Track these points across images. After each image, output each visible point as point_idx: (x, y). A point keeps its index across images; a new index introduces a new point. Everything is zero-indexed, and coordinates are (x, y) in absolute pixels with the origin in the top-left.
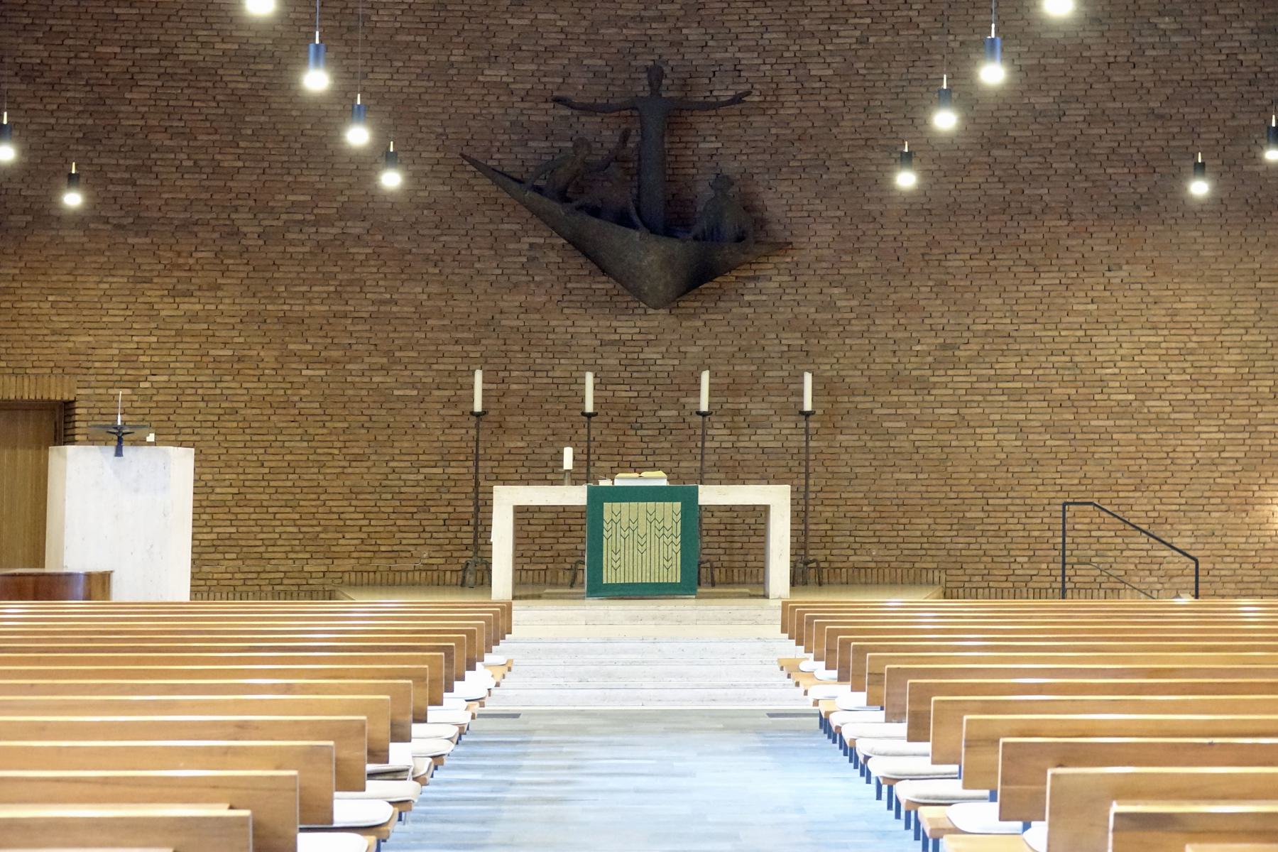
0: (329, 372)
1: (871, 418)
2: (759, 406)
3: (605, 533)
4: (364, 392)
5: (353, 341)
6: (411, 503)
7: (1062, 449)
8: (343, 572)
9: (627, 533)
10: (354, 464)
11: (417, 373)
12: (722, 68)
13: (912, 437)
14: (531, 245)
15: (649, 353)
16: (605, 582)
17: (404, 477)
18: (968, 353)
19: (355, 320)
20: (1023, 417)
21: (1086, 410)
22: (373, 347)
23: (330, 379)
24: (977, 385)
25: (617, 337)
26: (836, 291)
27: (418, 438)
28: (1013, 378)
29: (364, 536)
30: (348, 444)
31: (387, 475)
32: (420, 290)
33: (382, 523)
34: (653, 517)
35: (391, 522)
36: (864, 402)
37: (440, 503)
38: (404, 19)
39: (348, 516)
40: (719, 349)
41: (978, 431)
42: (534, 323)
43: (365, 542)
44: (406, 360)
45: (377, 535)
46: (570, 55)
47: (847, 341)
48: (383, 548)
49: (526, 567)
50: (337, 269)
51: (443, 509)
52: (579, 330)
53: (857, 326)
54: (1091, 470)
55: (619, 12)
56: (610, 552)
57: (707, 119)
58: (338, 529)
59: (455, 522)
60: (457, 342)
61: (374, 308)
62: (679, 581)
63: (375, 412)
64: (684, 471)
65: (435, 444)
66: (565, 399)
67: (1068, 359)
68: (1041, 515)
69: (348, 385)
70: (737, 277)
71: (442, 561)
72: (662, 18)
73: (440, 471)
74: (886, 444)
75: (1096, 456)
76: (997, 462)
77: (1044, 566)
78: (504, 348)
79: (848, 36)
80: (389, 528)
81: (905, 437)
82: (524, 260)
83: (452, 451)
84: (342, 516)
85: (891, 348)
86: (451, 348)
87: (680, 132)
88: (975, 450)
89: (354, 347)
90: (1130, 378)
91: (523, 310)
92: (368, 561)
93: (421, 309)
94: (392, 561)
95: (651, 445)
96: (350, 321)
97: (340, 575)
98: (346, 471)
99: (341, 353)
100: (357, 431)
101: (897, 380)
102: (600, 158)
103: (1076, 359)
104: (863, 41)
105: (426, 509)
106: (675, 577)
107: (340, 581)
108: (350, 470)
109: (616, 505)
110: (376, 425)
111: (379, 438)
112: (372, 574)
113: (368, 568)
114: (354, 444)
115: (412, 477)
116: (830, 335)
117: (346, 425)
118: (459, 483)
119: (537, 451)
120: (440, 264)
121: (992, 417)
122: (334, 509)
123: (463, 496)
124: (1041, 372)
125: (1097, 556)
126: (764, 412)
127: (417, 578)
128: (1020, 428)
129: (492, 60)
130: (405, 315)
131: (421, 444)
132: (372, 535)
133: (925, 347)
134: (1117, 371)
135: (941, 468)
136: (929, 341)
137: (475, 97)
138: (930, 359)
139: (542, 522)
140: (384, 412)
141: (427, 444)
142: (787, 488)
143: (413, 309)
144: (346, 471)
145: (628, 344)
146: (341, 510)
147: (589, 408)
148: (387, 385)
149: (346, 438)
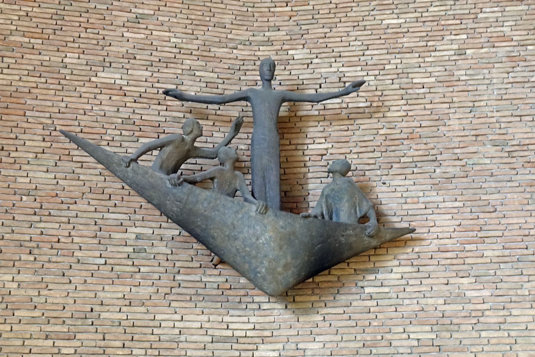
12: (327, 80)
14: (138, 237)
25: (229, 333)
26: (465, 281)
32: (10, 278)
38: (20, 23)
40: (342, 345)
42: (139, 316)
46: (184, 67)
47: (484, 334)
52: (187, 324)
53: (492, 318)
57: (316, 124)
70: (355, 270)
72: (270, 42)
78: (102, 343)
82: (131, 249)
86: (40, 342)
87: (289, 136)
91: (127, 302)
102: (211, 146)
104: (461, 53)
116: (463, 327)
120: (36, 251)
129: (106, 65)
137: (87, 95)
145: (241, 340)
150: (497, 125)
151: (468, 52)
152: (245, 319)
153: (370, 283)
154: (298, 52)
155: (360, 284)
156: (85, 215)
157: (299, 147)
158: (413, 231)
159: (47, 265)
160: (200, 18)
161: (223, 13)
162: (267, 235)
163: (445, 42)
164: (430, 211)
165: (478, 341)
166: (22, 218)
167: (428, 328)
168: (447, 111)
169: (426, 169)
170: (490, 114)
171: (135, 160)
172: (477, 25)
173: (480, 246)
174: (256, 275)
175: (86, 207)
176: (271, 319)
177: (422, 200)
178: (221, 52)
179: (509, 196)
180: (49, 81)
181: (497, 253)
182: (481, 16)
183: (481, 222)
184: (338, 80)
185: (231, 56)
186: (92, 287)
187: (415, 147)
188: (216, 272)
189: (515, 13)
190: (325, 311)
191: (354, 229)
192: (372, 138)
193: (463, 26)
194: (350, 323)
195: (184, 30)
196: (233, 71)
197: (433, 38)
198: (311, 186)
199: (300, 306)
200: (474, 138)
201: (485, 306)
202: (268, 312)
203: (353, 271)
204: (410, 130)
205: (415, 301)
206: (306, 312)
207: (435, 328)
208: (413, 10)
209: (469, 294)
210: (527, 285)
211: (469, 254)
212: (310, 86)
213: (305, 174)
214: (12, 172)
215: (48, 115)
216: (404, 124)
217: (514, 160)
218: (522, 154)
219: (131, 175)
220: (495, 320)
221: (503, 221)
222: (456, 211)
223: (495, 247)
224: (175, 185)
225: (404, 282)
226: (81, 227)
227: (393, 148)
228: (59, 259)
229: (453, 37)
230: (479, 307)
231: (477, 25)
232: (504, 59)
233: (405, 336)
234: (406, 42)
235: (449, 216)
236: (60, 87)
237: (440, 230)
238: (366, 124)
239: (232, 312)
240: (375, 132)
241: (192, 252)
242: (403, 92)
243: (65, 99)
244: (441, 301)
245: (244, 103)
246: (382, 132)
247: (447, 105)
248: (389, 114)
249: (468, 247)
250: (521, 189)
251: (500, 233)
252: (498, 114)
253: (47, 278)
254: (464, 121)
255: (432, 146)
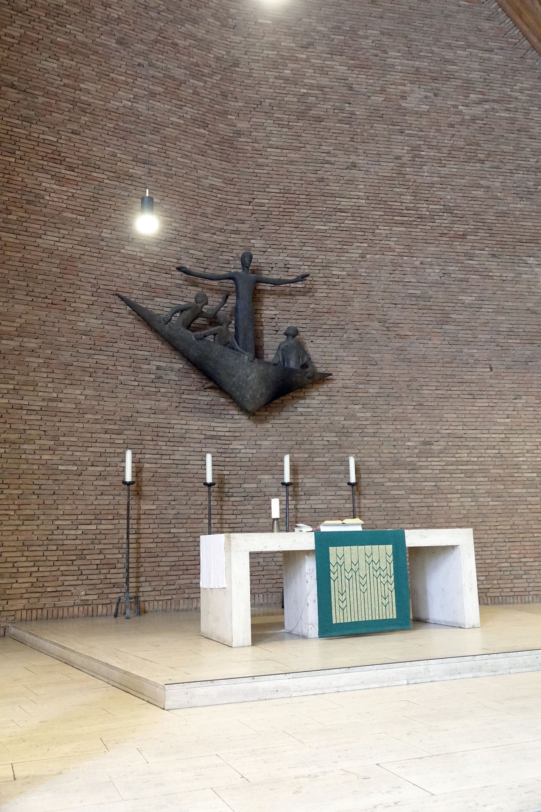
0: (7, 450)
1: (383, 488)
2: (311, 480)
3: (332, 575)
4: (35, 467)
5: (27, 428)
6: (72, 553)
7: (499, 507)
8: (16, 610)
9: (350, 574)
10: (26, 523)
11: (76, 453)
13: (409, 500)
14: (158, 368)
15: (236, 445)
16: (334, 622)
17: (66, 532)
18: (439, 447)
19: (29, 412)
20: (474, 487)
21: (510, 483)
22: (42, 433)
23: (8, 456)
24: (446, 467)
26: (356, 407)
27: (77, 502)
28: (467, 463)
29: (35, 580)
30: (22, 507)
31: (52, 531)
33: (49, 569)
34: (370, 559)
35: (55, 568)
36: (378, 478)
37: (93, 552)
39: (20, 564)
40: (283, 442)
41: (449, 496)
42: (161, 421)
43: (35, 585)
44: (69, 444)
45: (45, 579)
47: (365, 439)
48: (49, 589)
49: (157, 598)
50: (16, 372)
51: (96, 557)
54: (517, 520)
55: (211, 224)
56: (337, 593)
58: (13, 575)
59: (105, 566)
60: (106, 433)
61: (45, 404)
62: (395, 617)
63: (44, 482)
64: (262, 525)
65: (91, 507)
66: (182, 475)
67: (497, 451)
68: (490, 549)
69: (22, 461)
71: (96, 597)
72: (237, 232)
73: (94, 527)
74: (393, 505)
75: (519, 511)
76: (462, 516)
77: (495, 582)
79: (355, 253)
80: (54, 573)
81: (404, 500)
83: (103, 512)
84: (16, 565)
85: (392, 443)
86: (102, 436)
88: (447, 508)
89: (28, 432)
90: (533, 463)
92: (37, 600)
93: (79, 406)
94: (56, 599)
95: (239, 508)
96: (25, 412)
97: (13, 613)
98: (19, 528)
99: (18, 436)
100: (30, 497)
101: (397, 464)
103: (503, 451)
104: (363, 256)
105: (82, 556)
106: (391, 613)
107: (13, 618)
108: (23, 528)
109: (340, 549)
110: (45, 492)
111: (46, 502)
112: (39, 611)
113: (37, 607)
114: (27, 507)
115: (73, 532)
117: (20, 492)
118: (108, 537)
119: (164, 512)
120: (94, 375)
121: (457, 487)
122: (9, 559)
123: (111, 546)
124: (482, 459)
125: (525, 574)
126: (314, 485)
127: (76, 612)
128: (473, 495)
130: (68, 410)
131: (79, 507)
132: (40, 579)
133: (413, 443)
134: (525, 459)
135: (428, 520)
136: (416, 439)
138: (417, 451)
139: (168, 564)
140: (50, 482)
141: (84, 507)
142: (471, 530)
143: (74, 406)
144: (19, 528)
146: (16, 559)
147: (209, 480)
148: (54, 462)
149: (20, 502)
150: (382, 309)
151: (368, 256)
152: (224, 425)
153: (301, 405)
154: (258, 241)
155: (295, 406)
156: (124, 351)
157: (258, 312)
158: (331, 374)
159: (102, 385)
160: (191, 208)
161: (207, 206)
162: (253, 375)
163: (353, 247)
164: (338, 362)
165: (361, 443)
166: (83, 351)
167: (334, 434)
168: (352, 296)
169: (338, 334)
170: (378, 301)
171: (170, 320)
172: (374, 238)
173: (367, 386)
174: (243, 399)
175: (122, 346)
176: (240, 425)
177: (334, 354)
178: (205, 236)
179: (385, 355)
180: (93, 250)
181: (376, 391)
182: (377, 231)
183: (368, 371)
184: (284, 266)
185: (212, 240)
186: (131, 401)
187: (331, 318)
188: (206, 394)
189: (398, 233)
190: (274, 421)
191: (301, 373)
192: (304, 310)
193: (365, 237)
194: (288, 430)
195: (181, 217)
196: (213, 252)
197: (346, 244)
198: (265, 339)
199: (259, 418)
200: (367, 316)
201: (367, 423)
202: (238, 421)
203: (291, 398)
204: (329, 307)
205: (327, 418)
206: (262, 421)
207: (338, 434)
208: (334, 221)
209: (359, 415)
210: (391, 411)
211: (360, 390)
212: (266, 268)
213: (262, 330)
214: (74, 318)
215: (94, 276)
216: (325, 302)
217: (390, 333)
218: (395, 329)
219: (167, 329)
220: (372, 431)
221: (381, 371)
222: (354, 363)
223: (375, 387)
224: (198, 339)
225: (321, 406)
226: (121, 359)
227: (318, 318)
228: (109, 381)
229: (359, 244)
230: (364, 423)
231: (374, 238)
232: (389, 264)
233: (320, 438)
234: (330, 243)
235: (350, 366)
236: (100, 256)
237: (344, 374)
238: (302, 300)
239: (216, 420)
240: (307, 305)
241: (191, 380)
242: (326, 279)
243: (105, 265)
244: (343, 418)
245: (232, 281)
246: (311, 306)
247: (352, 292)
248: (316, 294)
249: (360, 386)
250: (391, 352)
251: (378, 379)
252: (383, 301)
253: (103, 394)
254: (363, 304)
255: (342, 319)
